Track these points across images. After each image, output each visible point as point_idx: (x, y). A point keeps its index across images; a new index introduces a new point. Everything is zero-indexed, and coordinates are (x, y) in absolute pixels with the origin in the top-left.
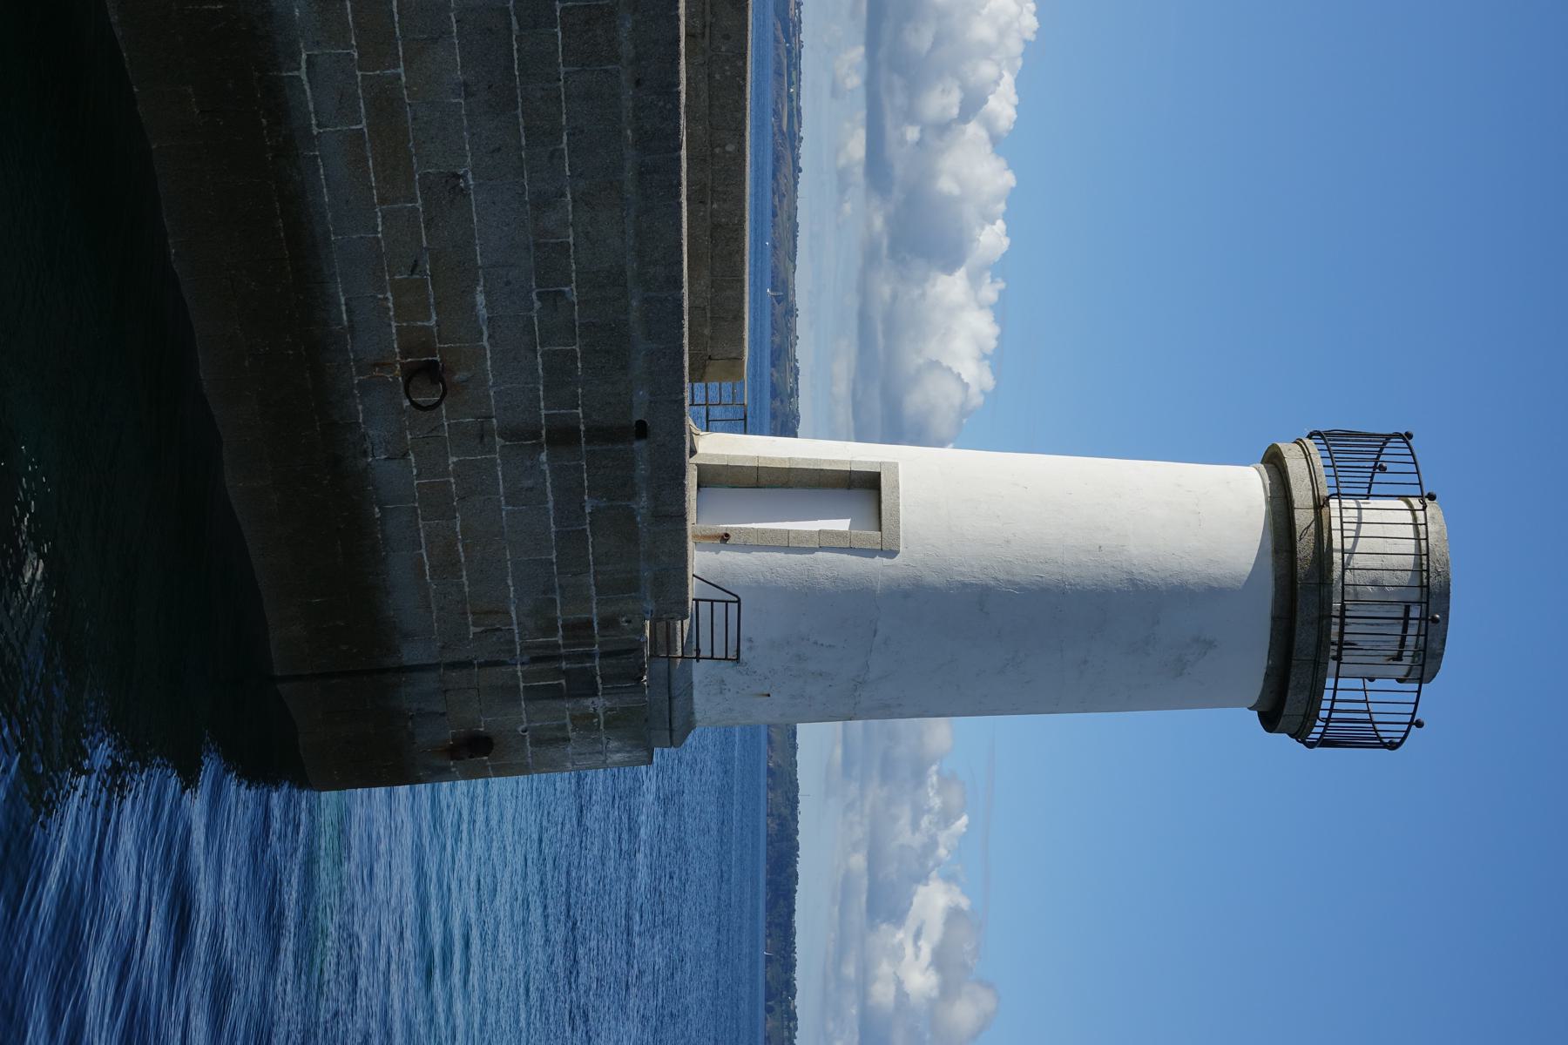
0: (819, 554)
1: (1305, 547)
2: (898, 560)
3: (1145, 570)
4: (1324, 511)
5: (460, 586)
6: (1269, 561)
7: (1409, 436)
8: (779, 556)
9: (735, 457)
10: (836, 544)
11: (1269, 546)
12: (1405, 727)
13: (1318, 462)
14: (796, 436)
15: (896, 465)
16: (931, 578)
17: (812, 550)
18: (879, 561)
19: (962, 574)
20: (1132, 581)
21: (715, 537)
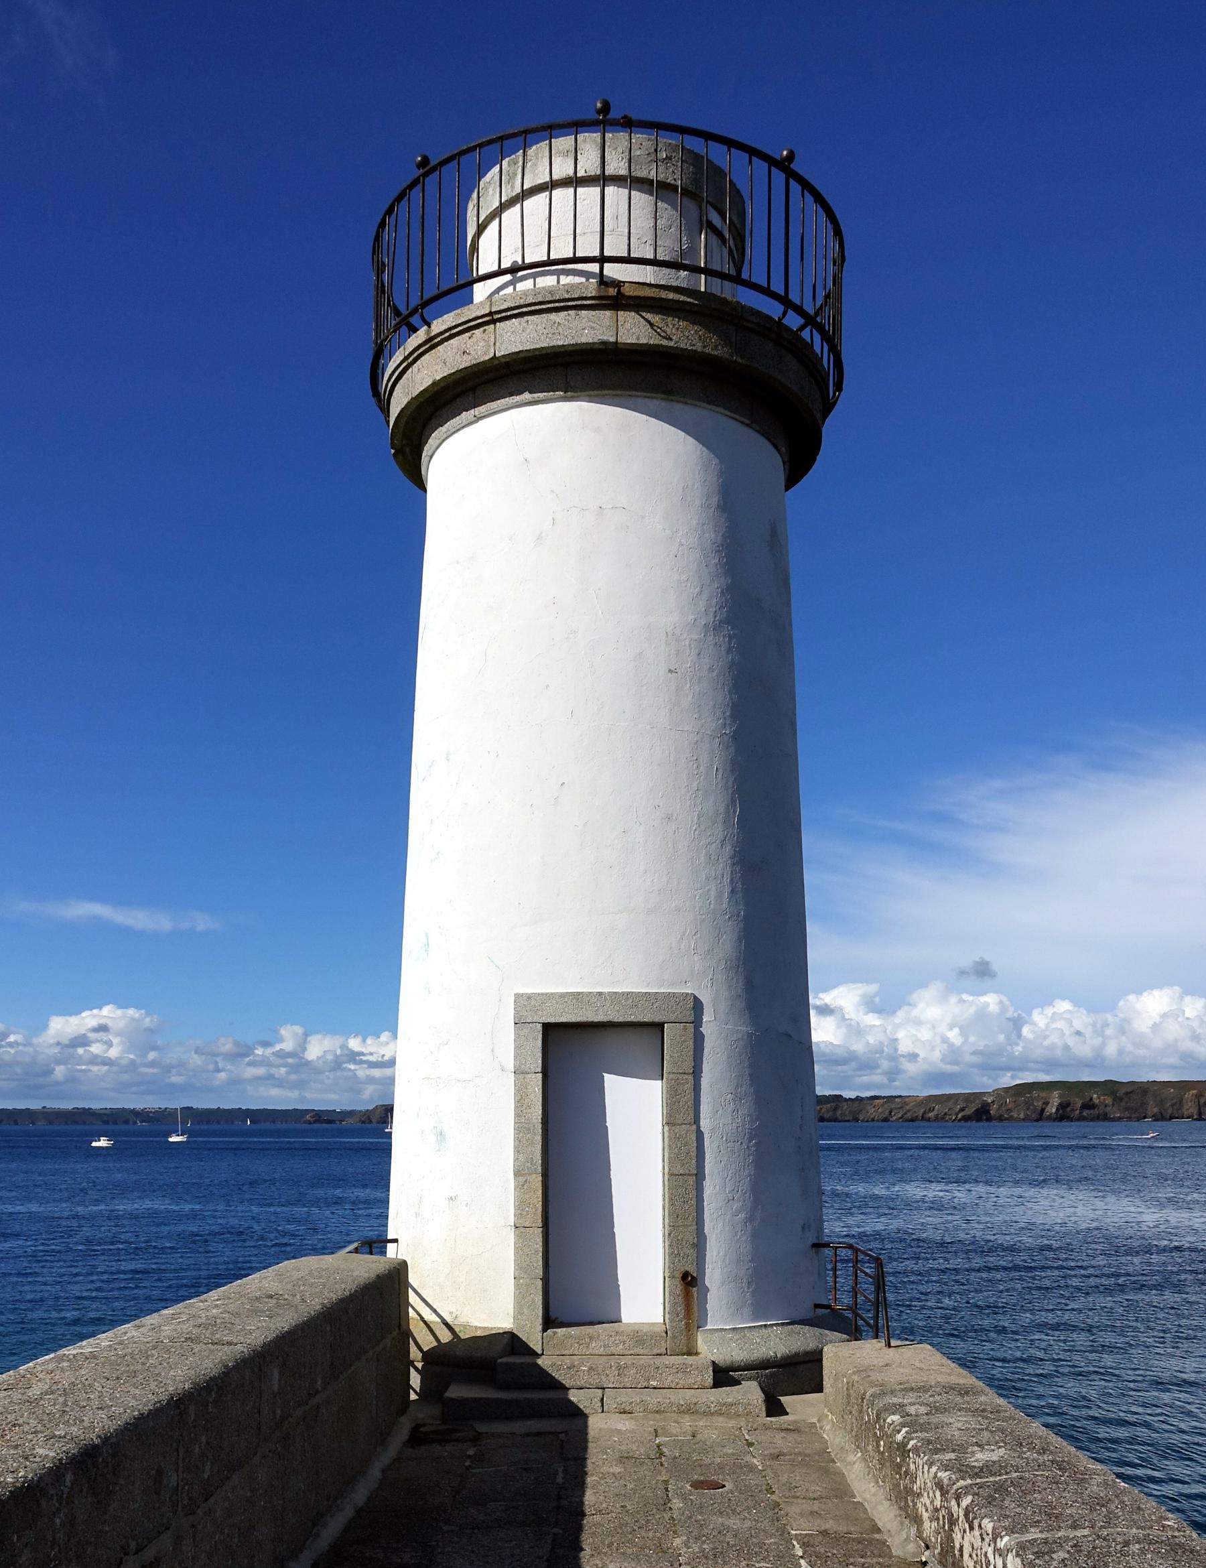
0: (704, 1123)
1: (683, 335)
2: (705, 999)
3: (702, 605)
4: (628, 291)
5: (565, 1471)
6: (678, 408)
7: (425, 161)
8: (710, 1188)
9: (519, 1266)
10: (690, 1096)
11: (656, 404)
12: (778, 287)
13: (398, 357)
14: (386, 1113)
15: (518, 996)
16: (727, 946)
17: (700, 1135)
18: (709, 1026)
19: (720, 895)
20: (717, 627)
21: (687, 1297)
